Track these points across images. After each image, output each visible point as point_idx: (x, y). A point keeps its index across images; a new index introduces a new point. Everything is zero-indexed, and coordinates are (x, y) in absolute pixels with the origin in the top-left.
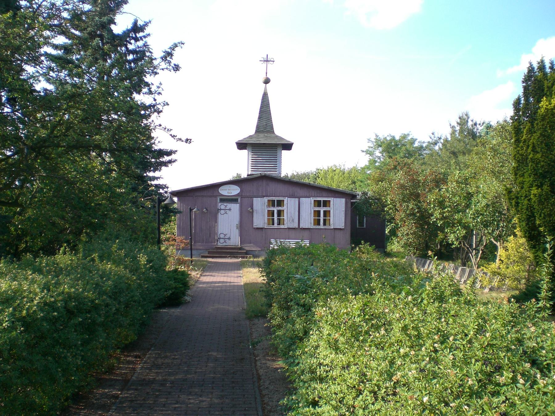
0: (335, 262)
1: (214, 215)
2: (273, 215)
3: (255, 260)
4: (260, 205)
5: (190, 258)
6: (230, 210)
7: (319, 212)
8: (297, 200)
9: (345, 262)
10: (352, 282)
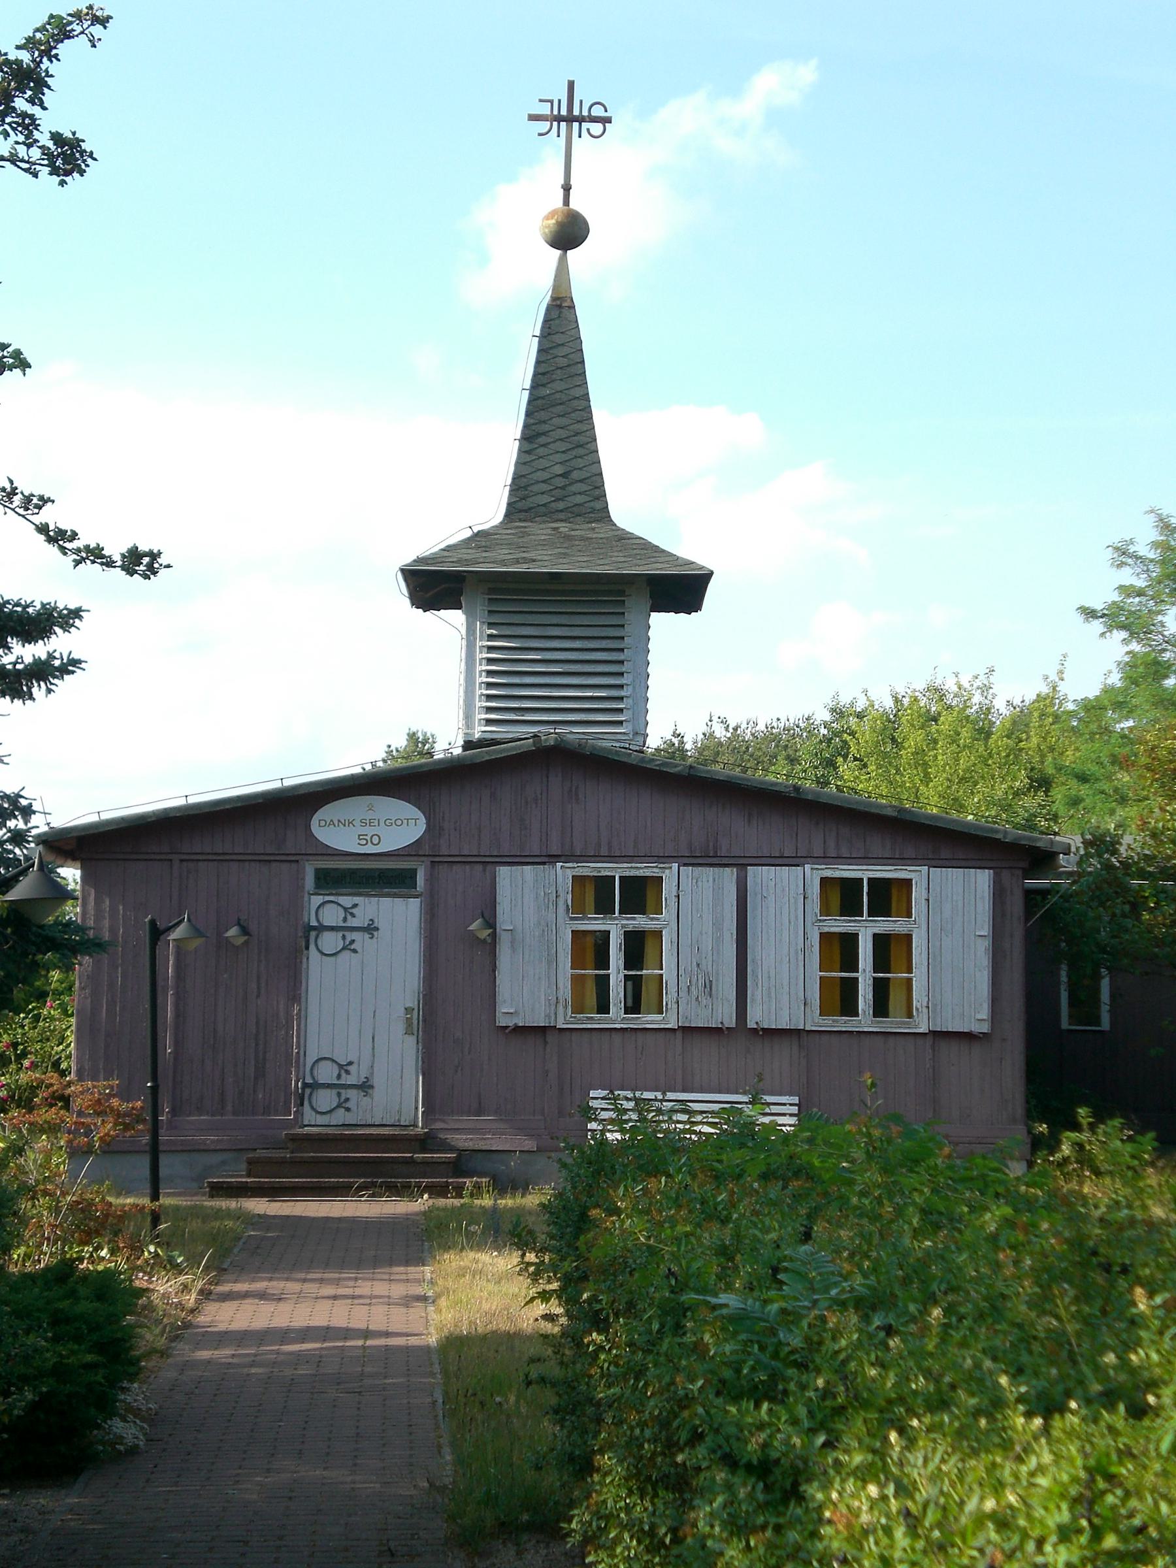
0: (932, 1220)
1: (282, 958)
3: (507, 1202)
4: (533, 903)
5: (145, 1201)
6: (370, 929)
7: (849, 942)
8: (729, 876)
9: (990, 1221)
10: (1027, 1339)
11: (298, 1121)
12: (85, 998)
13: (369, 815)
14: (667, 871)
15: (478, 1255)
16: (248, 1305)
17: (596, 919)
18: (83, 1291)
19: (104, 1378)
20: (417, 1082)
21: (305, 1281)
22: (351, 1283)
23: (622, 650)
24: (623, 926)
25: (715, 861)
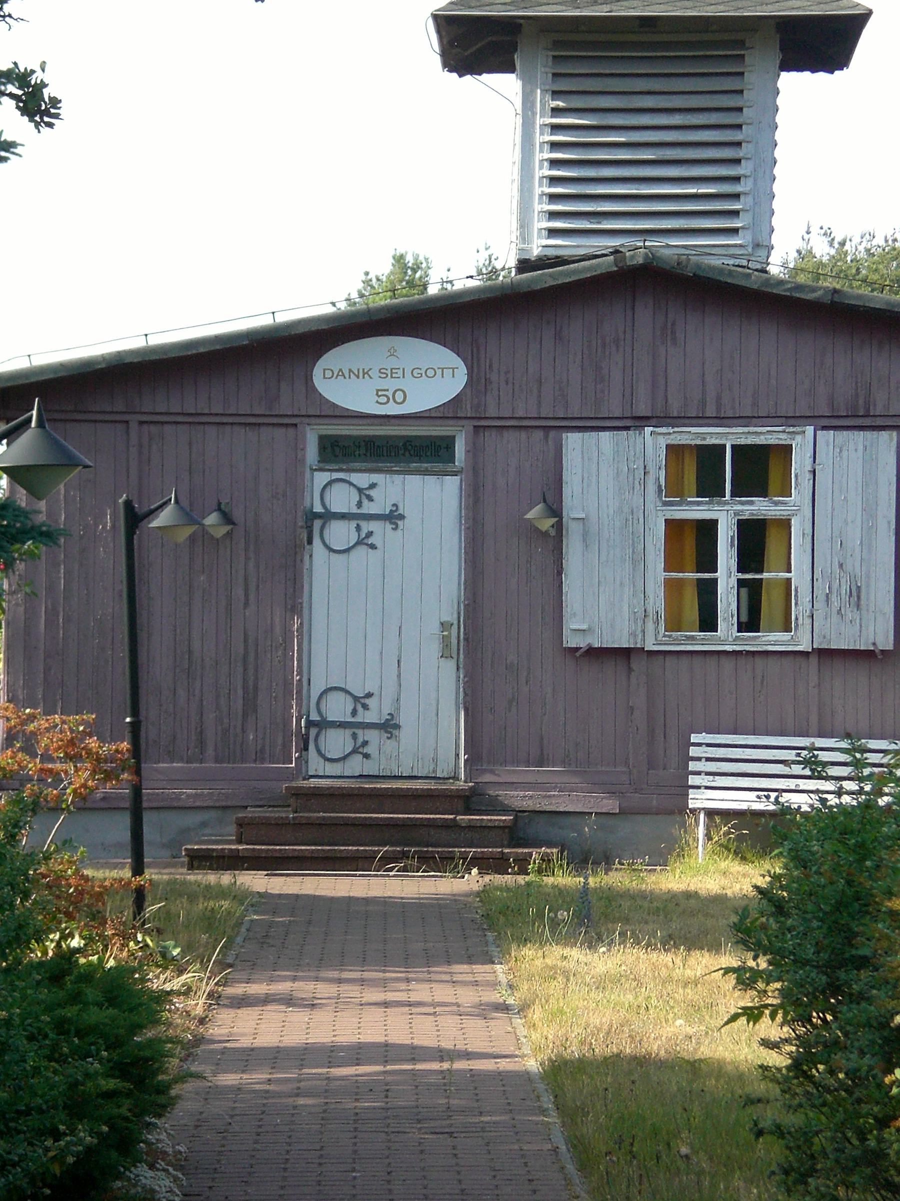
1: (279, 553)
2: (707, 561)
4: (614, 484)
6: (393, 517)
11: (301, 771)
12: (17, 605)
13: (392, 363)
14: (799, 438)
15: (567, 951)
16: (273, 1013)
17: (699, 504)
18: (91, 994)
19: (130, 1110)
20: (458, 721)
21: (340, 981)
22: (403, 986)
23: (739, 127)
24: (736, 513)
25: (867, 422)
